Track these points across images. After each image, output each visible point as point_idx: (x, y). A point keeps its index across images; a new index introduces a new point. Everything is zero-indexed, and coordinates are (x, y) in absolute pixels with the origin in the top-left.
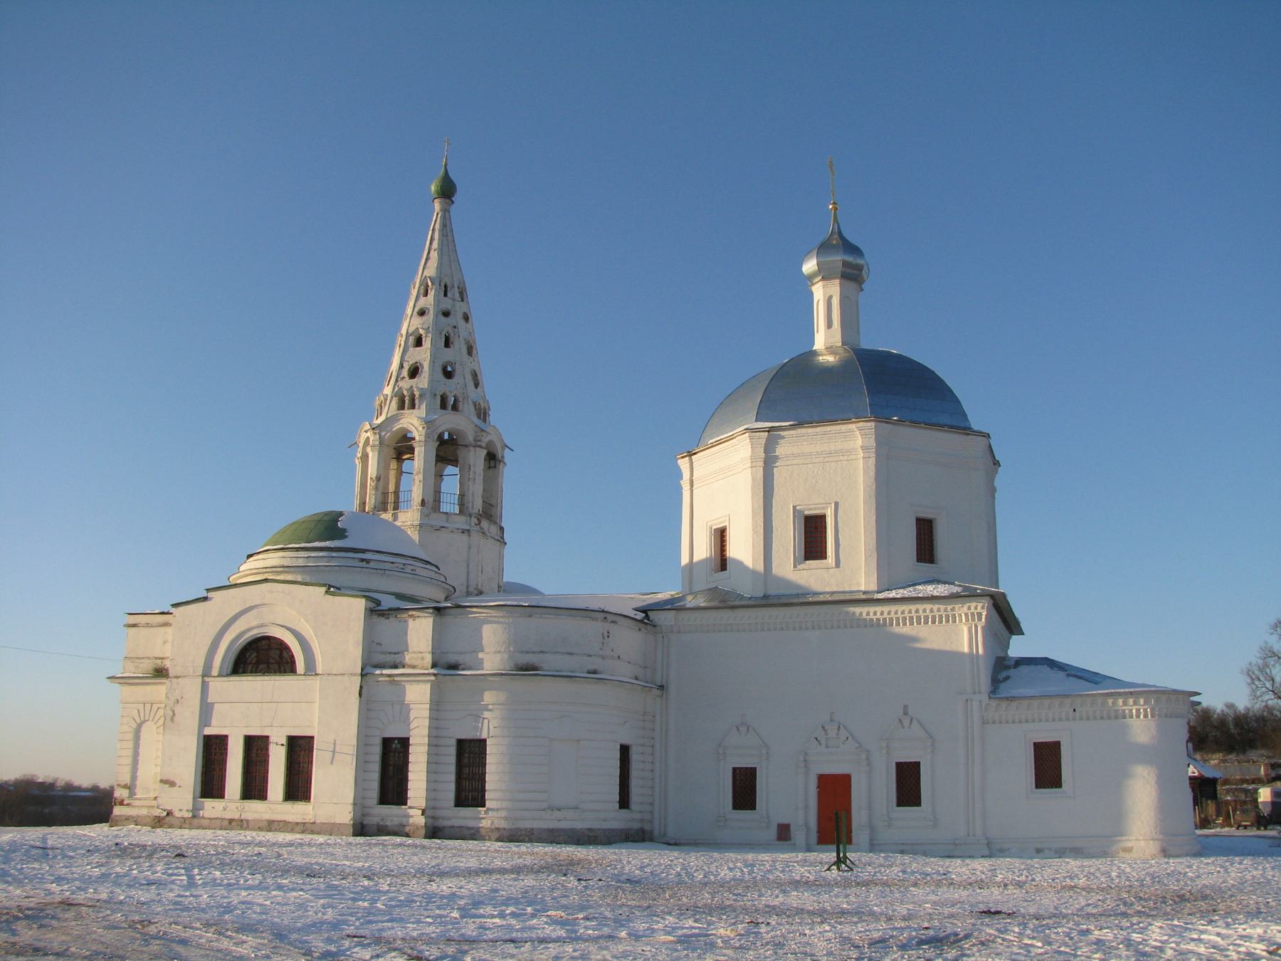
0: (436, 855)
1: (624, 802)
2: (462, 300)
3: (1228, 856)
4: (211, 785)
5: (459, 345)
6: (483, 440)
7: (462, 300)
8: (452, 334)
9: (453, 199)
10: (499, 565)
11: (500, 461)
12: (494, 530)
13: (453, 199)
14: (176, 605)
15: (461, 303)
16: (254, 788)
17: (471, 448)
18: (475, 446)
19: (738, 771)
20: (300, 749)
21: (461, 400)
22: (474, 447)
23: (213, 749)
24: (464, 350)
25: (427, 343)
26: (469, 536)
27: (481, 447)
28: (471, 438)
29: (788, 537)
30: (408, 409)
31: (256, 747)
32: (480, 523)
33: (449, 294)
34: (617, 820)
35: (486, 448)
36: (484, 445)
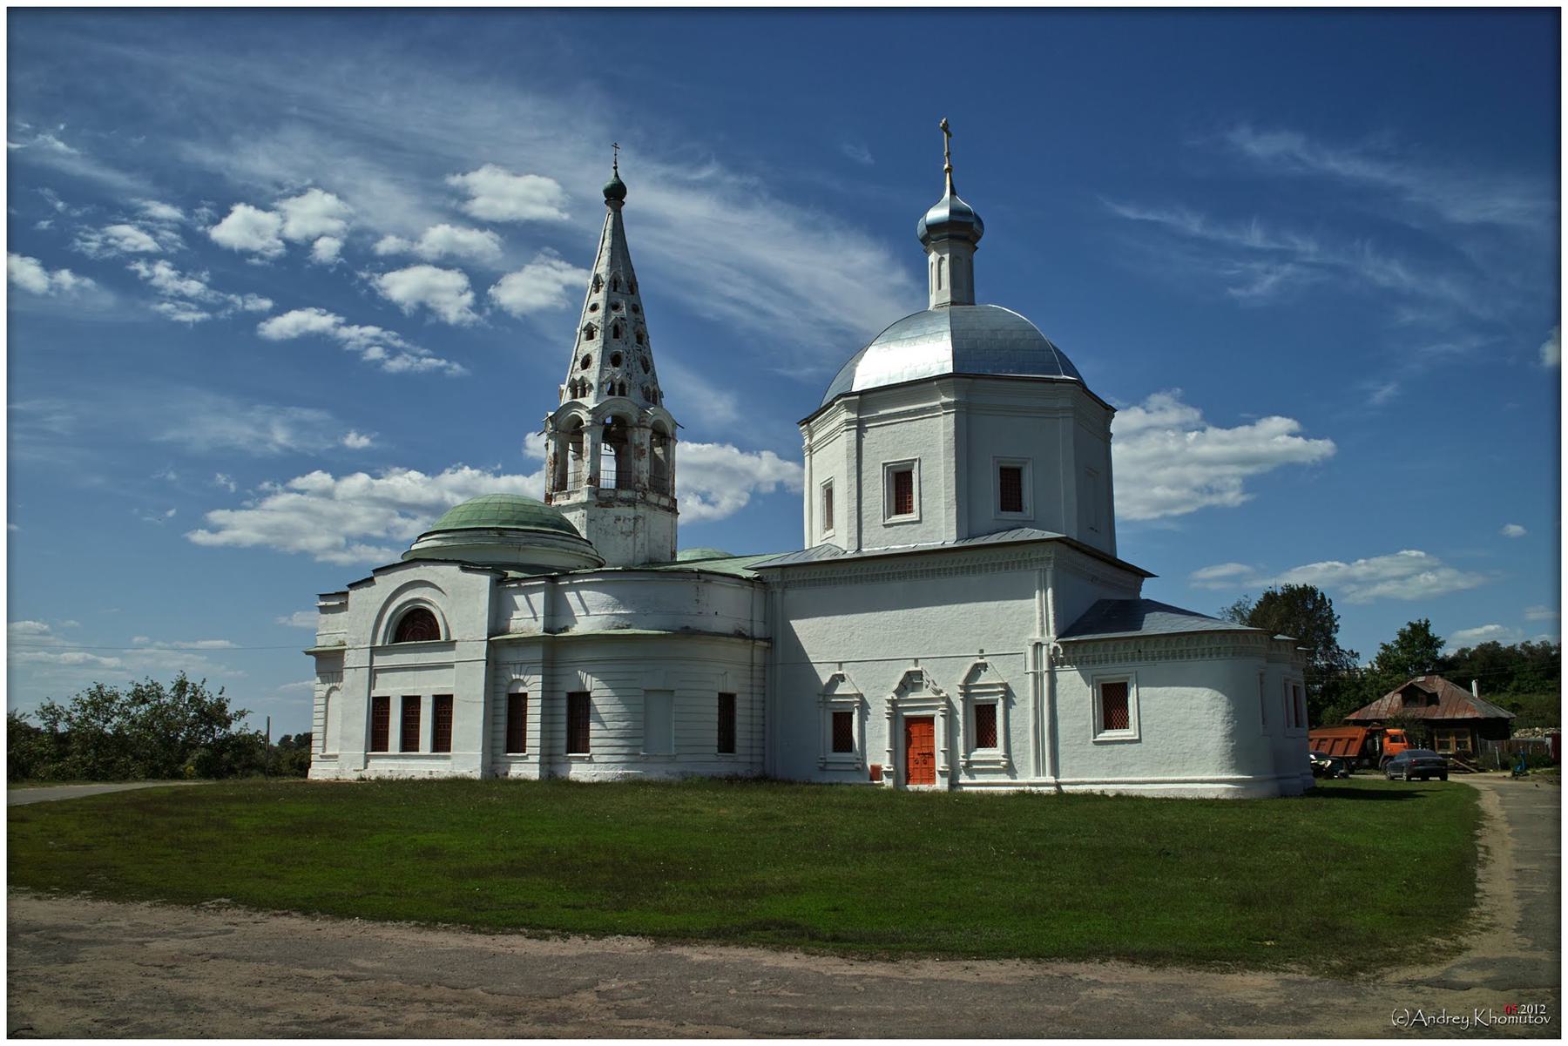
0: (1119, 879)
1: (727, 742)
2: (632, 293)
3: (1349, 560)
4: (377, 741)
5: (628, 334)
6: (647, 420)
7: (632, 293)
8: (620, 325)
9: (624, 200)
10: (672, 533)
11: (670, 439)
12: (665, 502)
13: (624, 200)
14: (352, 586)
15: (631, 296)
16: (409, 742)
17: (636, 429)
18: (639, 426)
19: (924, 727)
20: (443, 704)
21: (627, 385)
22: (637, 427)
23: (379, 707)
24: (633, 339)
25: (598, 335)
26: (635, 508)
27: (645, 427)
28: (635, 420)
29: (877, 491)
30: (581, 397)
31: (411, 704)
32: (645, 496)
33: (618, 289)
34: (724, 766)
35: (651, 428)
36: (648, 425)
